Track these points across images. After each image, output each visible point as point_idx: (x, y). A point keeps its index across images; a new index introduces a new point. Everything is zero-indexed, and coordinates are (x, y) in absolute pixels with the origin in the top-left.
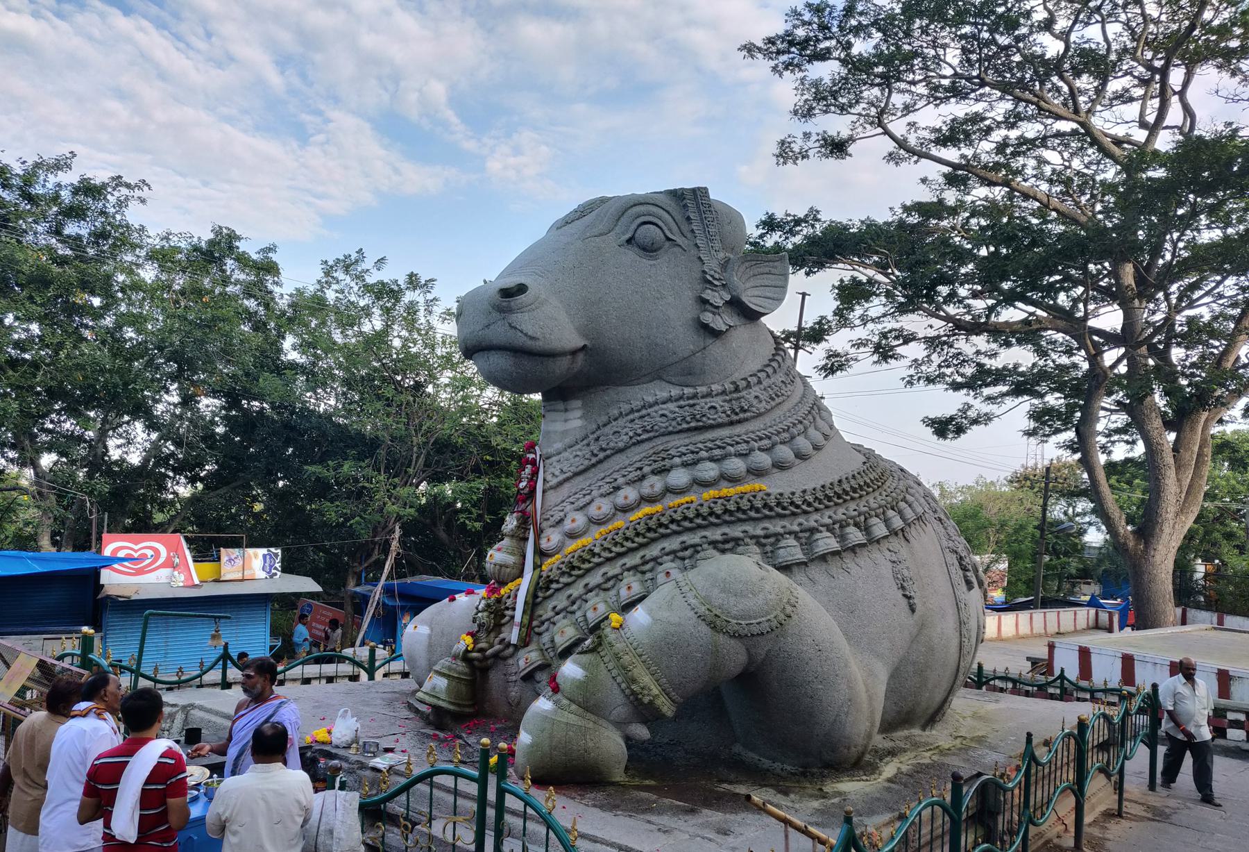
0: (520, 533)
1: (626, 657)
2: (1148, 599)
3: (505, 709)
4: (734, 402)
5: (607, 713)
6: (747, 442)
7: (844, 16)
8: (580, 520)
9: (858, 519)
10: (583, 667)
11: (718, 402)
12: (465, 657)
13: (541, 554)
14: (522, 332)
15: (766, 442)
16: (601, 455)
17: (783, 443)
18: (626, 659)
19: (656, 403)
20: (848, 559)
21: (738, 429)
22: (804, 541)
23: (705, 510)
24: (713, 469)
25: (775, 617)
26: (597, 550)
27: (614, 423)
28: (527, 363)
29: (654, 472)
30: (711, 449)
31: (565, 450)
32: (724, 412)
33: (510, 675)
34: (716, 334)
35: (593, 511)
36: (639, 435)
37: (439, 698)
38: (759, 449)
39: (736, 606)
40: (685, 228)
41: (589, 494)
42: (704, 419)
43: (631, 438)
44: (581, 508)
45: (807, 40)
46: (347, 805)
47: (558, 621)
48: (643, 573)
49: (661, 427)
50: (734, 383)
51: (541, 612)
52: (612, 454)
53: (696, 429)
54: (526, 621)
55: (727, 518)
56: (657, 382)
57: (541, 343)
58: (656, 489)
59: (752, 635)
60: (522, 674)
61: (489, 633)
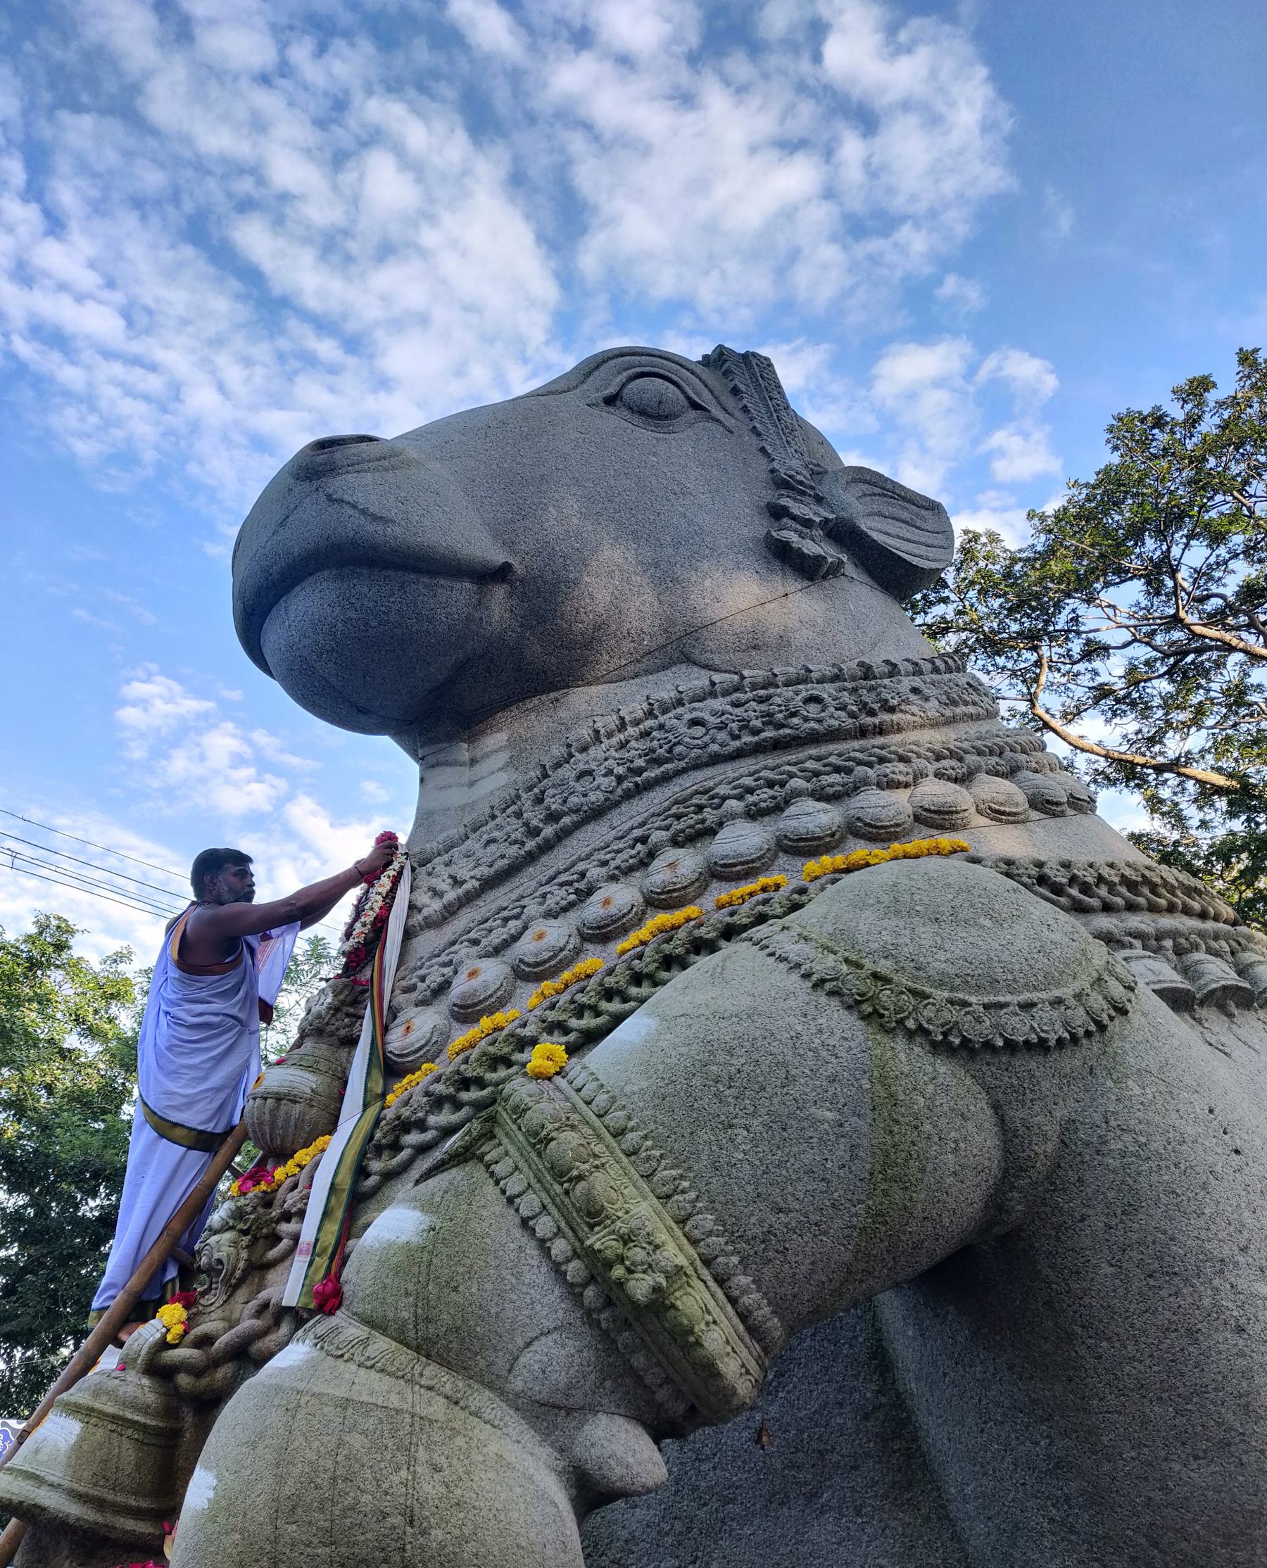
0: (341, 1025)
1: (567, 1135)
5: (501, 1363)
8: (492, 972)
14: (354, 507)
16: (549, 831)
25: (1078, 996)
28: (367, 589)
29: (675, 842)
30: (817, 774)
32: (843, 708)
35: (527, 948)
40: (730, 402)
41: (517, 917)
42: (795, 720)
43: (620, 779)
53: (777, 746)
54: (330, 1238)
57: (398, 531)
58: (681, 870)
59: (1011, 1046)
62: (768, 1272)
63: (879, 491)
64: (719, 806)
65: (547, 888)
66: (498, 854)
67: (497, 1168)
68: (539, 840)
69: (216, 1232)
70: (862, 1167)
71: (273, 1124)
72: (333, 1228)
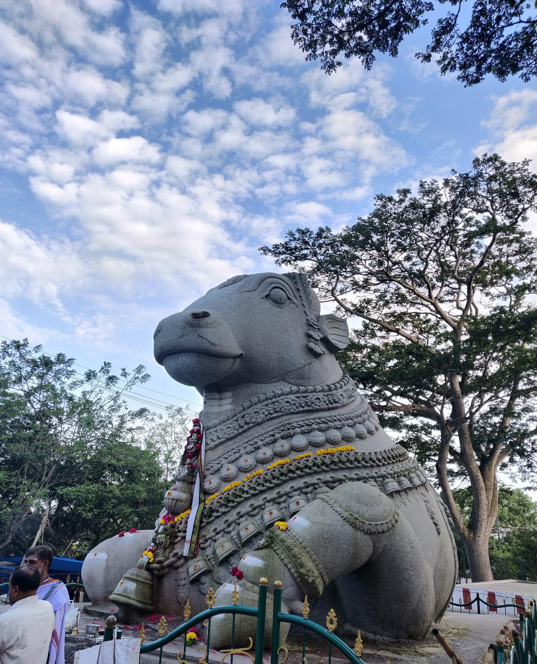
1: (295, 549)
2: (478, 566)
3: (175, 606)
4: (329, 396)
6: (340, 420)
7: (316, 237)
8: (233, 469)
9: (405, 473)
10: (263, 558)
11: (320, 395)
12: (148, 568)
13: (205, 492)
14: (207, 340)
15: (350, 421)
16: (246, 427)
17: (360, 423)
18: (296, 550)
19: (282, 394)
20: (414, 491)
21: (333, 413)
22: (380, 483)
23: (319, 461)
24: (322, 436)
26: (246, 489)
27: (254, 406)
28: (206, 362)
29: (282, 438)
30: (319, 423)
31: (220, 424)
32: (325, 402)
33: (181, 580)
34: (317, 355)
35: (242, 463)
36: (272, 414)
37: (129, 598)
38: (347, 425)
39: (368, 512)
41: (238, 452)
42: (313, 405)
43: (266, 416)
44: (233, 462)
45: (296, 248)
46: (130, 649)
47: (218, 539)
48: (279, 503)
49: (286, 409)
50: (328, 386)
51: (205, 533)
52: (253, 427)
53: (308, 411)
54: (194, 539)
55: (333, 466)
56: (282, 382)
57: (218, 348)
58: (285, 448)
59: (378, 532)
60: (191, 578)
61: (165, 549)
62: (330, 575)
63: (332, 320)
64: (294, 429)
65: (246, 445)
66: (231, 432)
67: (278, 552)
68: (243, 429)
69: (160, 534)
70: (350, 556)
71: (175, 507)
72: (195, 537)
